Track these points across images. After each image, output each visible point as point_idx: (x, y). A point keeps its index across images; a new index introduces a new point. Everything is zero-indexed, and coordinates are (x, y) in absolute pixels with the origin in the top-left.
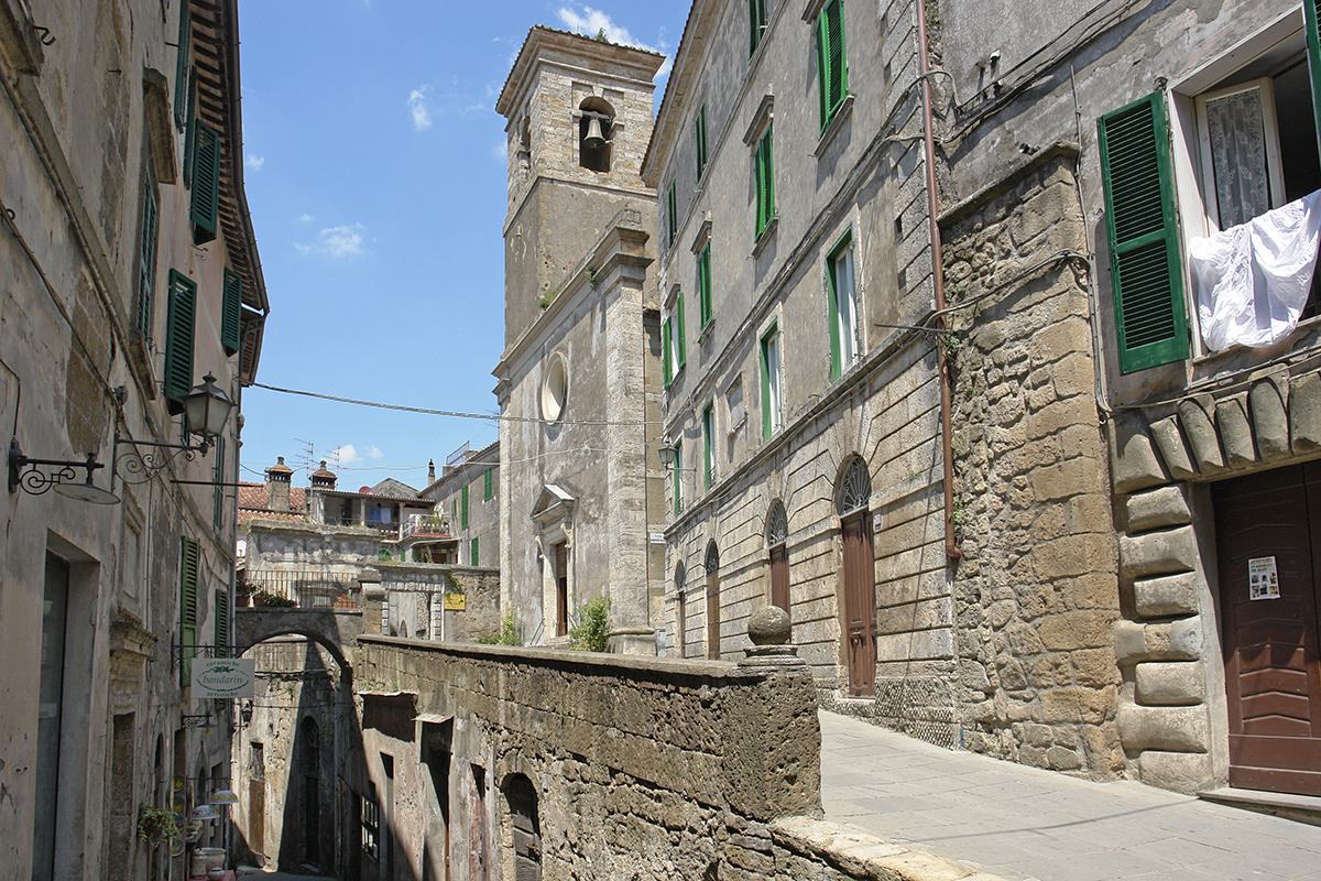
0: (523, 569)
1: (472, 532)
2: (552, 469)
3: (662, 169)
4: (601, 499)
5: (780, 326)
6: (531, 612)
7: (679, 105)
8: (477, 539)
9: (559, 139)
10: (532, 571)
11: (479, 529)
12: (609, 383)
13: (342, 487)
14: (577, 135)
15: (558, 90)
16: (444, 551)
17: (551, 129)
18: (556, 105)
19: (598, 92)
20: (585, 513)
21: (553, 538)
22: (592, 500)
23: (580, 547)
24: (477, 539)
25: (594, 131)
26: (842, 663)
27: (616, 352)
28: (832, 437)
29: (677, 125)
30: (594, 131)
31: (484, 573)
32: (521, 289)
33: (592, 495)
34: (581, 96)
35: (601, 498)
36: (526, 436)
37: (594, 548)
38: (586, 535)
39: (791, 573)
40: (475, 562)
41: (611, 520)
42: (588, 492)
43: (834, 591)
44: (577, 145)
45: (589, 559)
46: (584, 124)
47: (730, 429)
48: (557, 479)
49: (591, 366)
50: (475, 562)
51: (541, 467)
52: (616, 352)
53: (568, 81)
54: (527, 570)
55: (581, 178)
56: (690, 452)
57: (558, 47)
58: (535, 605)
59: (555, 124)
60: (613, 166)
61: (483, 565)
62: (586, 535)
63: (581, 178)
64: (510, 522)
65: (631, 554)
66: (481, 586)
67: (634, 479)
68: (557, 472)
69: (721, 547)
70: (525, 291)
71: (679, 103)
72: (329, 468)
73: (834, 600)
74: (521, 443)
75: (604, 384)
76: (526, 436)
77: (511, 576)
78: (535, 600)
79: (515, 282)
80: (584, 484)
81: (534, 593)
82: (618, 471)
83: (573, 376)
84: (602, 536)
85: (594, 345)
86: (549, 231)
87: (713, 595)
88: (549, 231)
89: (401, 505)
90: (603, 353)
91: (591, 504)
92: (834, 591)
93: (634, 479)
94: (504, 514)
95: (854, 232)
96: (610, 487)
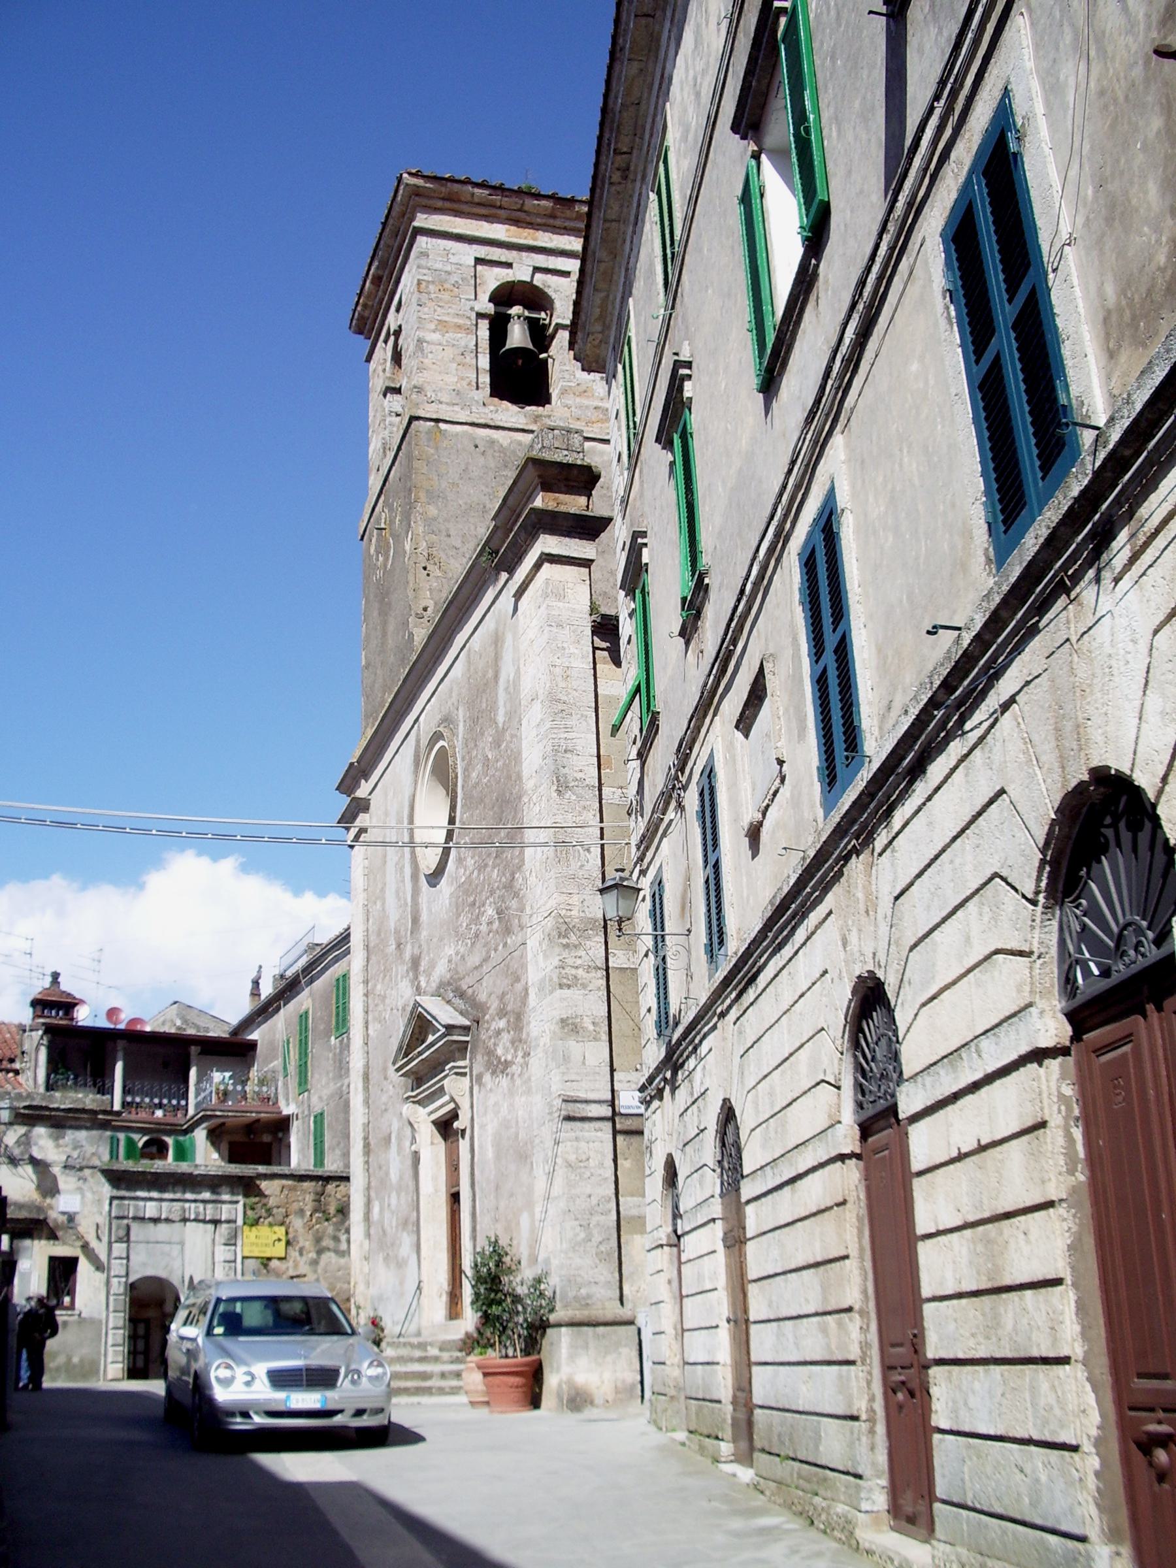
0: (387, 1174)
1: (315, 1099)
2: (432, 965)
3: (609, 328)
4: (517, 1020)
5: (843, 499)
6: (401, 1264)
7: (625, 178)
8: (322, 1114)
9: (449, 353)
10: (401, 1178)
11: (326, 1093)
12: (525, 774)
13: (84, 1016)
14: (485, 345)
15: (449, 273)
16: (266, 1138)
17: (435, 337)
18: (446, 296)
19: (521, 272)
20: (490, 1053)
21: (439, 1106)
22: (502, 1024)
23: (482, 1127)
24: (322, 1114)
25: (517, 336)
26: (1112, 1536)
27: (537, 706)
28: (1015, 748)
29: (626, 222)
30: (517, 336)
31: (327, 1179)
32: (385, 624)
33: (502, 1013)
34: (493, 278)
35: (519, 1017)
36: (391, 900)
37: (507, 1128)
38: (491, 1102)
39: (917, 1195)
40: (319, 1159)
41: (537, 1062)
42: (494, 1005)
43: (1064, 1272)
44: (485, 362)
45: (498, 1157)
46: (498, 327)
47: (750, 815)
48: (442, 985)
49: (497, 744)
50: (319, 1159)
51: (415, 962)
52: (537, 706)
53: (467, 254)
54: (394, 1176)
55: (494, 416)
56: (679, 895)
57: (448, 205)
58: (406, 1241)
59: (442, 326)
60: (554, 392)
61: (332, 1166)
62: (491, 1102)
63: (494, 416)
64: (366, 1078)
65: (577, 1139)
66: (319, 1206)
67: (580, 972)
68: (441, 970)
69: (746, 1119)
70: (391, 628)
71: (625, 171)
72: (66, 985)
73: (1064, 1300)
74: (383, 917)
75: (519, 777)
76: (391, 900)
77: (368, 1188)
78: (407, 1240)
79: (376, 613)
80: (487, 991)
81: (405, 1223)
82: (546, 957)
83: (466, 770)
84: (520, 1100)
85: (501, 703)
86: (432, 511)
87: (736, 1240)
88: (432, 511)
89: (194, 1050)
90: (514, 714)
91: (498, 1032)
92: (1064, 1272)
93: (580, 972)
94: (356, 1061)
95: (1019, 107)
96: (532, 992)
